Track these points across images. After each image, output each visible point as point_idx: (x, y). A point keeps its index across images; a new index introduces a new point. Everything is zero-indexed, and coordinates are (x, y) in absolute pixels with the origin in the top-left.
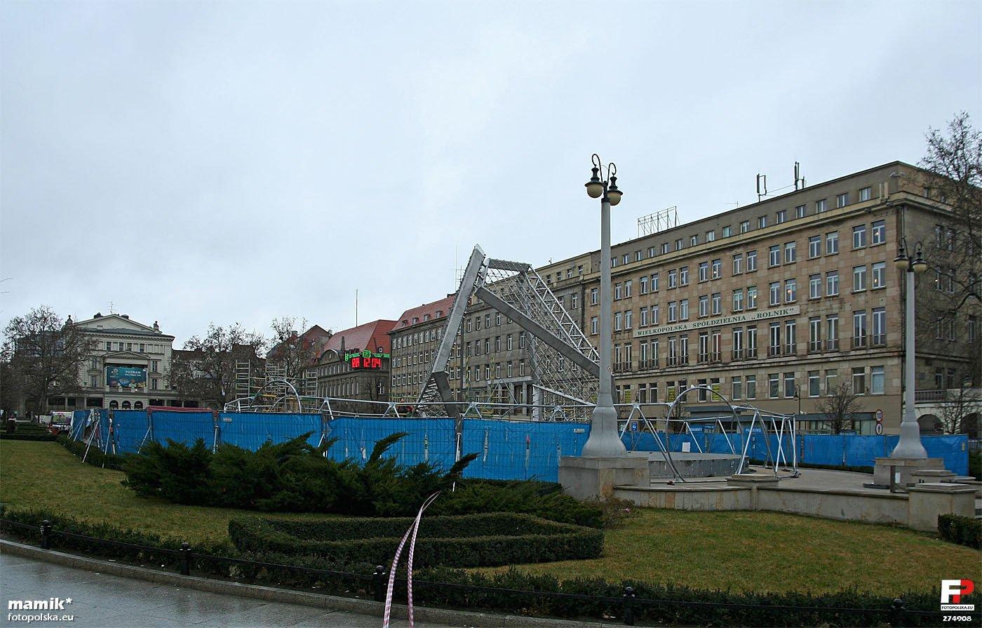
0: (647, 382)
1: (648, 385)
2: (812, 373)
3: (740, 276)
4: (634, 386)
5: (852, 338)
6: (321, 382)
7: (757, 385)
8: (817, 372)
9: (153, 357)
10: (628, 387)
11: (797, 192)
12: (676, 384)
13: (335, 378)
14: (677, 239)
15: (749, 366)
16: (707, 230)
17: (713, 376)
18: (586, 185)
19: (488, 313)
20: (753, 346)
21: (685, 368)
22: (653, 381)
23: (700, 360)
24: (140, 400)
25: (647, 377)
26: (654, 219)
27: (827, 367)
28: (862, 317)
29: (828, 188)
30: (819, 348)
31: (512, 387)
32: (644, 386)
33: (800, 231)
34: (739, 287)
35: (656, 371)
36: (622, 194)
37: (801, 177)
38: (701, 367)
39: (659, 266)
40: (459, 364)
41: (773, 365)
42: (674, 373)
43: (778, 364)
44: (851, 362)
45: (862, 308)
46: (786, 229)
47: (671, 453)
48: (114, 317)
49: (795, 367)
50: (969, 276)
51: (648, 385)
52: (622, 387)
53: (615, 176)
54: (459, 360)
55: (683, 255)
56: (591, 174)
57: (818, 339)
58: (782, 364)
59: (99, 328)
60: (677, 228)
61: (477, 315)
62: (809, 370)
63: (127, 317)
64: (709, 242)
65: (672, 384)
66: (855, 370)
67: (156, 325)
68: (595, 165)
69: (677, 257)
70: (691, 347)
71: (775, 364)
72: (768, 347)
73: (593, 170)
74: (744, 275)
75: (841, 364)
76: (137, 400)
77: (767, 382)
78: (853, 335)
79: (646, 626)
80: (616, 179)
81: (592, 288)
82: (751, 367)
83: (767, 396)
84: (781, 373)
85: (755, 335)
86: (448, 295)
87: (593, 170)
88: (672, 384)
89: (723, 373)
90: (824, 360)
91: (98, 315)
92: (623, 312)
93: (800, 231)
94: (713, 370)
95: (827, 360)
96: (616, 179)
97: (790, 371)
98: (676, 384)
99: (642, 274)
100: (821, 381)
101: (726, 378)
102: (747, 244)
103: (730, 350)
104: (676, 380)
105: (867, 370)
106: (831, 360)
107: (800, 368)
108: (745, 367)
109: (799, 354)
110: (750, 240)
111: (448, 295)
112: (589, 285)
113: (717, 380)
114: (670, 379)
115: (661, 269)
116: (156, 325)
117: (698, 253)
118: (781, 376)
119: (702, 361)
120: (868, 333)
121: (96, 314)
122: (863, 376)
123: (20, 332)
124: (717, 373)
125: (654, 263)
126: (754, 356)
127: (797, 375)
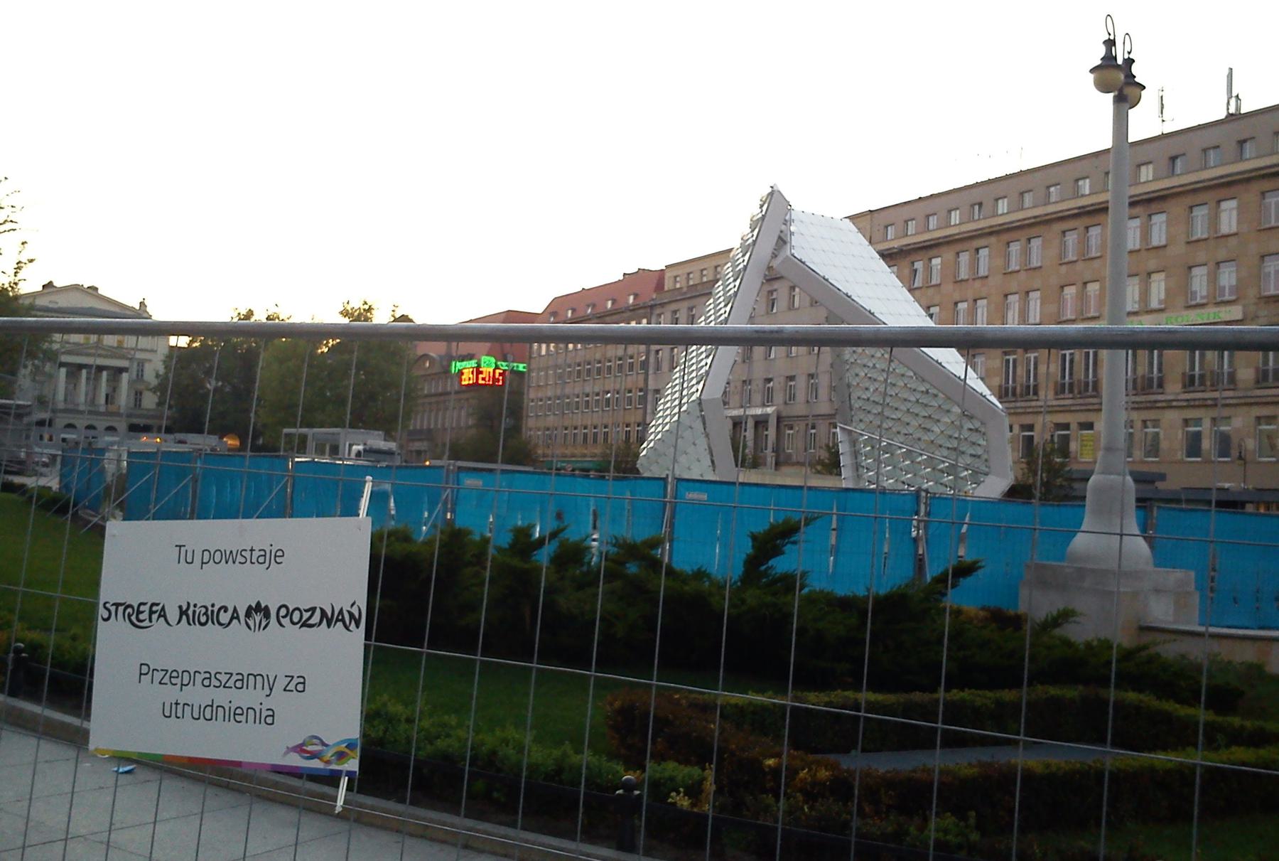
2: (1262, 421)
6: (460, 400)
7: (1162, 436)
8: (1198, 422)
9: (139, 355)
11: (1232, 118)
13: (433, 399)
17: (1083, 418)
18: (1092, 71)
19: (691, 305)
20: (1010, 382)
21: (1033, 404)
23: (1060, 389)
24: (71, 421)
27: (1214, 413)
30: (1014, 394)
31: (751, 424)
33: (1248, 180)
36: (1144, 88)
37: (1234, 94)
38: (1062, 402)
39: (991, 234)
40: (641, 384)
41: (1192, 403)
43: (1201, 403)
46: (1222, 177)
47: (1083, 528)
48: (76, 288)
53: (1131, 56)
54: (641, 378)
55: (1035, 217)
56: (1102, 51)
57: (1014, 381)
59: (51, 306)
61: (674, 307)
62: (1258, 414)
63: (96, 289)
64: (1083, 196)
66: (1186, 422)
67: (142, 304)
68: (1110, 34)
69: (1024, 219)
70: (1042, 369)
71: (1197, 403)
72: (1184, 374)
73: (1105, 42)
76: (89, 423)
77: (1180, 432)
79: (292, 767)
80: (1133, 61)
82: (1152, 406)
83: (1180, 455)
84: (1206, 416)
85: (1072, 361)
86: (625, 274)
87: (1105, 42)
91: (50, 285)
93: (1248, 180)
96: (1133, 61)
97: (1153, 418)
99: (959, 247)
100: (1071, 438)
102: (1150, 201)
103: (997, 384)
109: (1241, 385)
111: (625, 274)
115: (993, 239)
116: (142, 304)
118: (1207, 423)
119: (1063, 392)
121: (46, 282)
122: (1068, 435)
123: (1233, 209)
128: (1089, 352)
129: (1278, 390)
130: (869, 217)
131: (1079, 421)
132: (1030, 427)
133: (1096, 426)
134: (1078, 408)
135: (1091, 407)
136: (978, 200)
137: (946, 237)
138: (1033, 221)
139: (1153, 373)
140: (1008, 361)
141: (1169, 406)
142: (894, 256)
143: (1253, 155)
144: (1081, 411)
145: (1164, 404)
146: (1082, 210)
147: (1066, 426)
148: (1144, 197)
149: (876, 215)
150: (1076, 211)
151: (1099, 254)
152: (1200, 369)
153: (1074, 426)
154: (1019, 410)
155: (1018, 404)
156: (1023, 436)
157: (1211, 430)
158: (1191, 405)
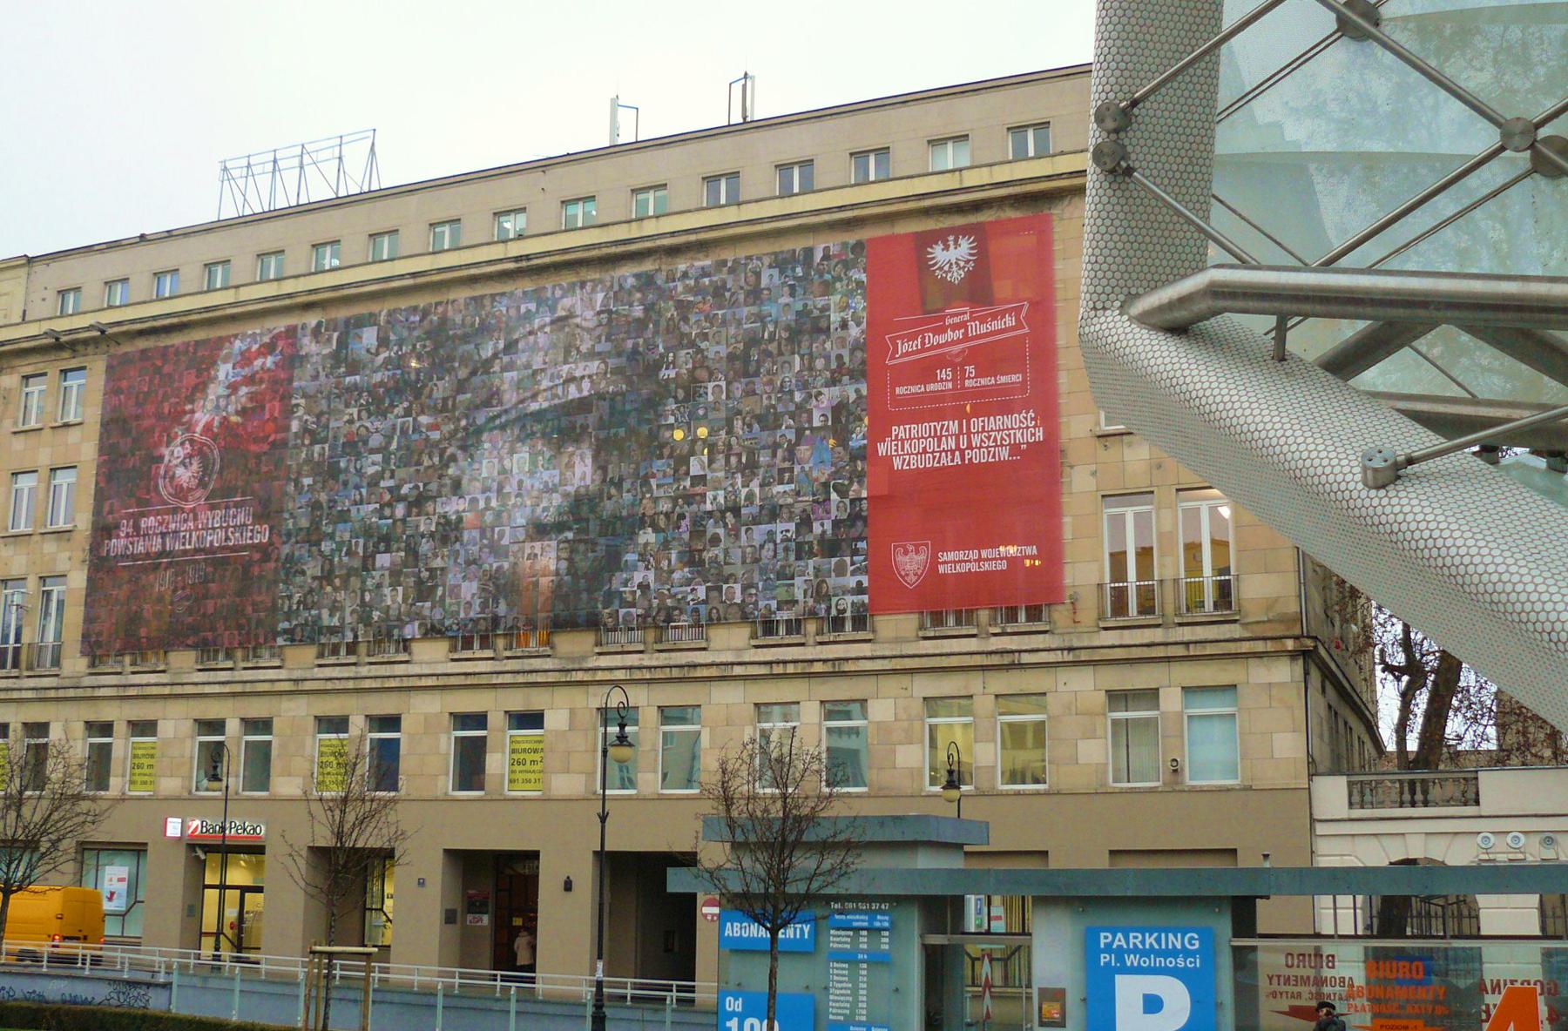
0: (232, 716)
1: (233, 726)
3: (32, 437)
4: (175, 724)
5: (1100, 586)
8: (1150, 696)
10: (144, 728)
12: (357, 724)
14: (209, 258)
15: (676, 673)
16: (501, 205)
17: (518, 701)
21: (400, 669)
22: (257, 709)
25: (234, 695)
26: (256, 170)
28: (1137, 515)
29: (413, 199)
32: (216, 726)
34: (28, 466)
35: (271, 674)
38: (328, 673)
42: (351, 684)
43: (800, 668)
44: (657, 687)
45: (1143, 485)
49: (1162, 667)
50: (427, 514)
51: (233, 726)
52: (120, 728)
55: (414, 275)
57: (17, 640)
58: (818, 667)
60: (639, 147)
65: (338, 724)
71: (791, 669)
74: (47, 432)
75: (1064, 675)
78: (1102, 577)
81: (29, 370)
83: (446, 783)
88: (338, 724)
89: (562, 694)
90: (995, 660)
92: (44, 472)
94: (521, 679)
95: (1007, 660)
98: (357, 724)
101: (572, 711)
104: (358, 713)
105: (1171, 700)
106: (1026, 658)
107: (891, 685)
108: (658, 674)
110: (693, 238)
112: (17, 362)
113: (532, 720)
114: (331, 707)
117: (473, 271)
120: (25, 639)
122: (221, 744)
124: (534, 691)
125: (290, 296)
126: (53, 665)
127: (881, 710)
128: (1123, 516)
129: (4, 686)
130: (23, 272)
131: (319, 714)
132: (391, 722)
133: (549, 720)
134: (508, 679)
135: (540, 678)
136: (729, 167)
137: (207, 309)
138: (410, 282)
139: (7, 642)
140: (48, 594)
141: (724, 675)
142: (80, 348)
143: (711, 205)
144: (895, 672)
145: (714, 672)
146: (524, 264)
147: (479, 720)
148: (667, 242)
149: (38, 268)
150: (511, 266)
151: (79, 420)
152: (1140, 577)
153: (496, 719)
154: (367, 684)
155: (364, 671)
156: (456, 738)
157: (820, 724)
158: (774, 673)
